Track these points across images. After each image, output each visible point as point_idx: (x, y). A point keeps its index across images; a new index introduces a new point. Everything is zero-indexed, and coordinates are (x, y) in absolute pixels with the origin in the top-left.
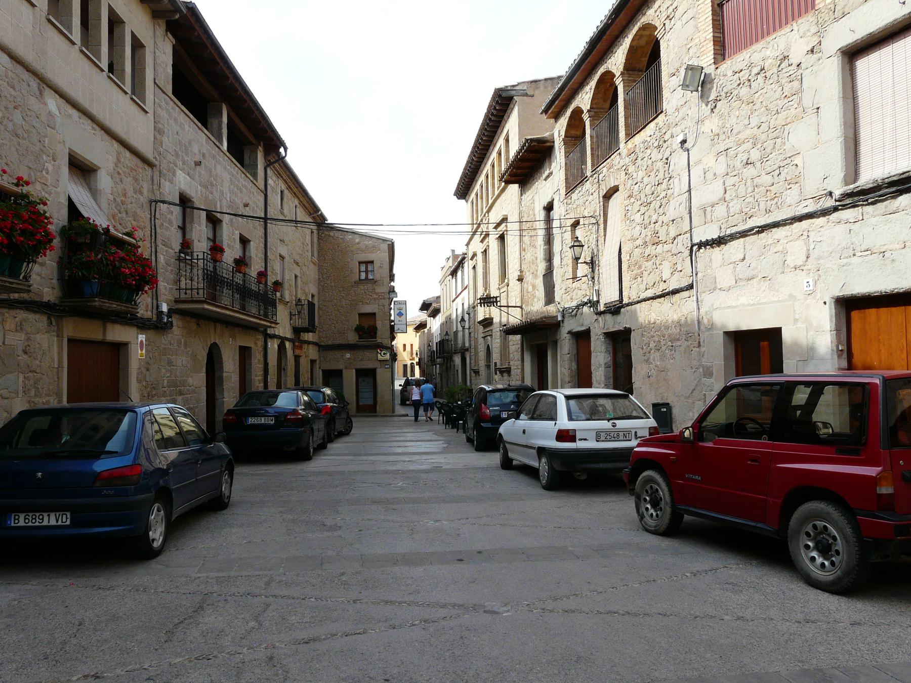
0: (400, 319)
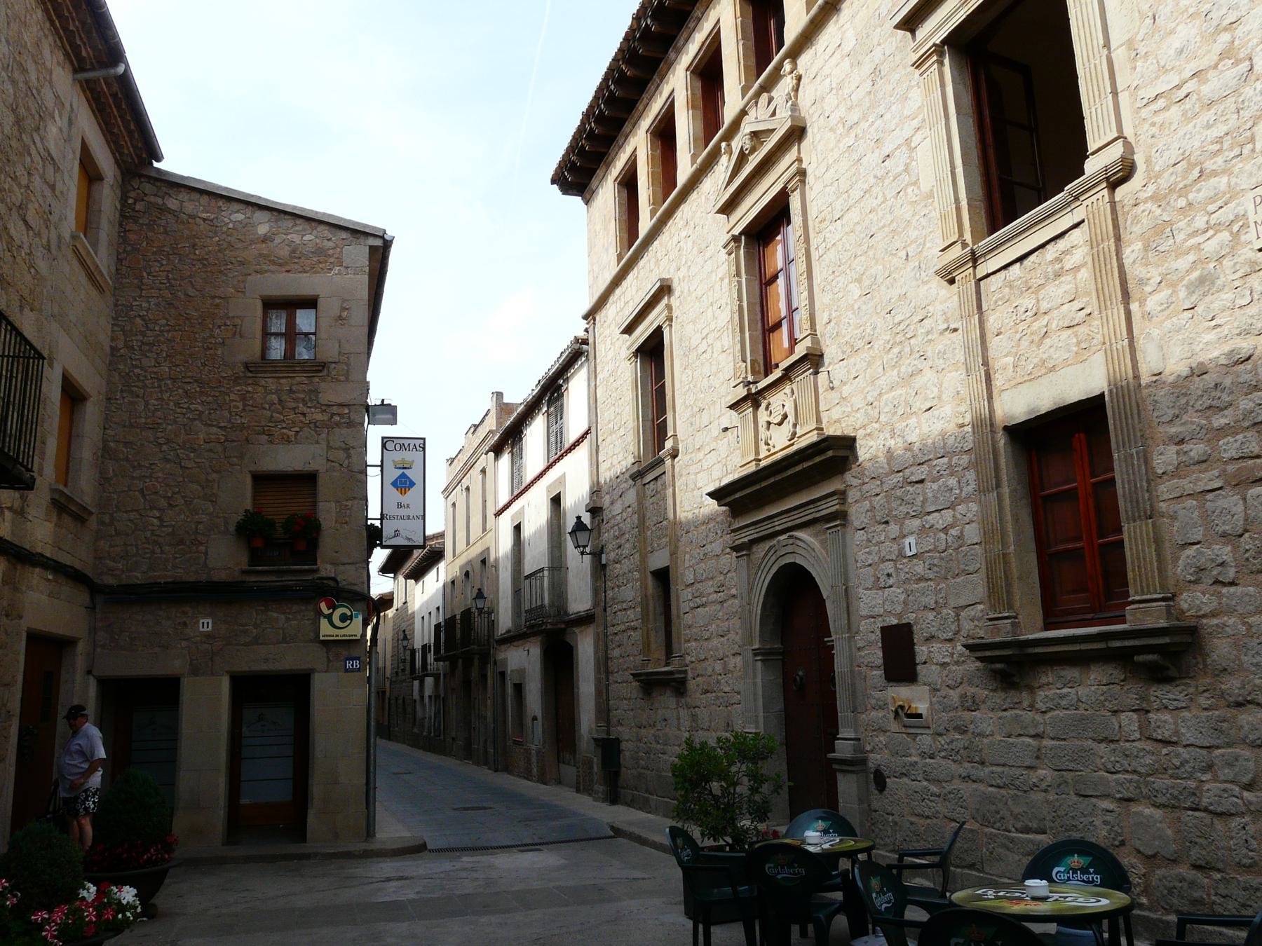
0: (404, 499)
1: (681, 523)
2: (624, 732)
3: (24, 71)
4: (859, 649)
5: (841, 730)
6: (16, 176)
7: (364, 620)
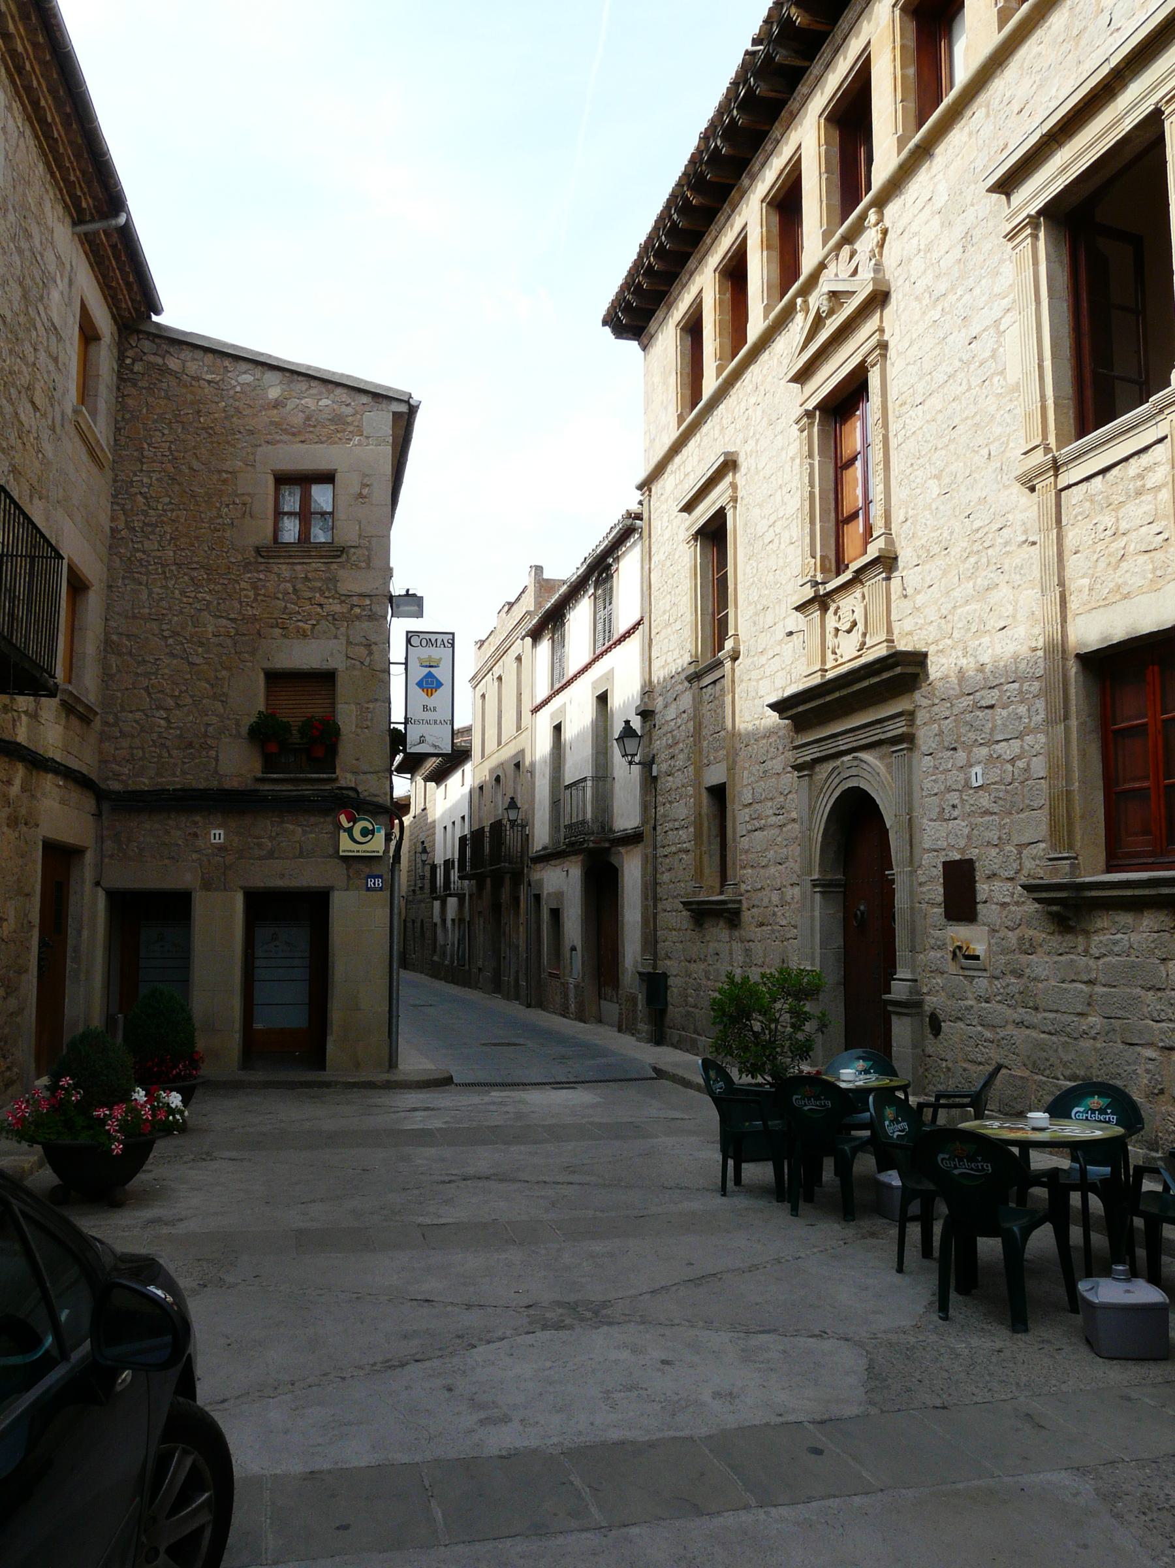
0: (431, 702)
1: (740, 734)
2: (671, 966)
3: (29, 236)
4: (921, 884)
5: (898, 970)
6: (24, 355)
7: (386, 835)
